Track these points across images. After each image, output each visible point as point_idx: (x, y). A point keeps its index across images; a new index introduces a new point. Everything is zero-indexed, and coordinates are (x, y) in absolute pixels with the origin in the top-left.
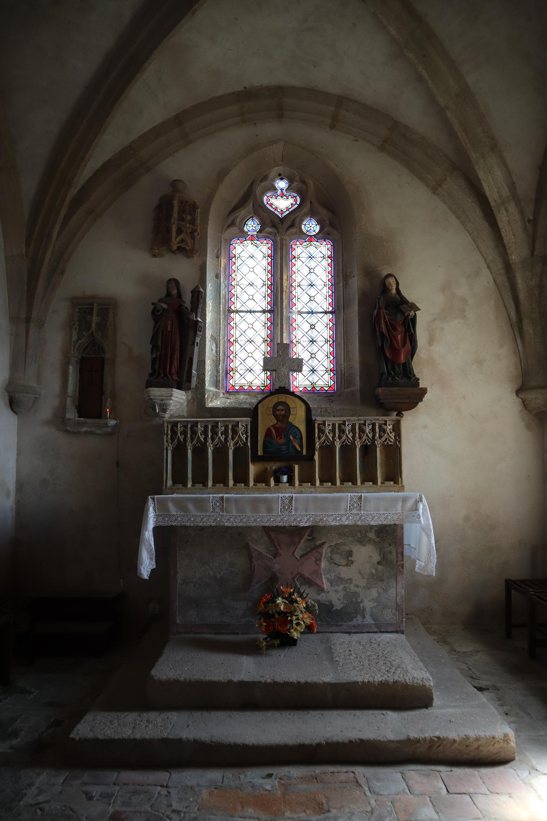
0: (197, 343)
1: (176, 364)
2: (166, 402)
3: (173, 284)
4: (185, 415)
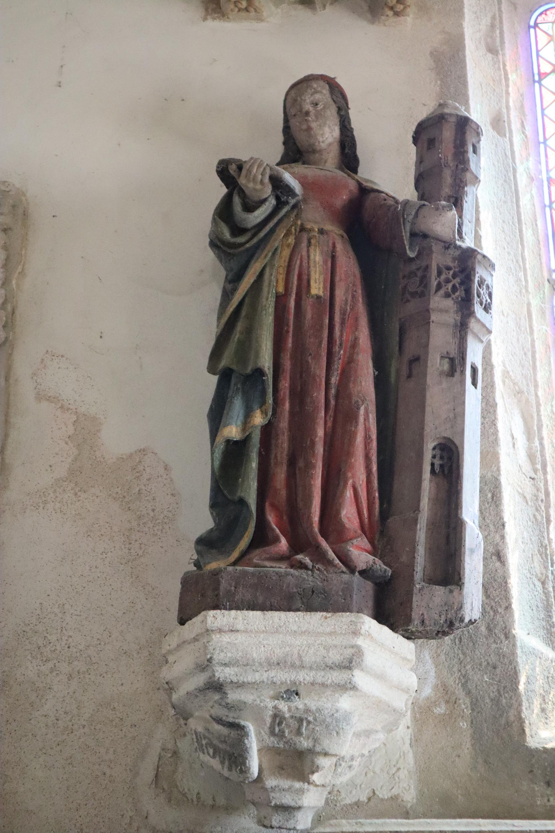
0: (474, 370)
1: (360, 473)
2: (306, 702)
3: (323, 95)
4: (410, 797)
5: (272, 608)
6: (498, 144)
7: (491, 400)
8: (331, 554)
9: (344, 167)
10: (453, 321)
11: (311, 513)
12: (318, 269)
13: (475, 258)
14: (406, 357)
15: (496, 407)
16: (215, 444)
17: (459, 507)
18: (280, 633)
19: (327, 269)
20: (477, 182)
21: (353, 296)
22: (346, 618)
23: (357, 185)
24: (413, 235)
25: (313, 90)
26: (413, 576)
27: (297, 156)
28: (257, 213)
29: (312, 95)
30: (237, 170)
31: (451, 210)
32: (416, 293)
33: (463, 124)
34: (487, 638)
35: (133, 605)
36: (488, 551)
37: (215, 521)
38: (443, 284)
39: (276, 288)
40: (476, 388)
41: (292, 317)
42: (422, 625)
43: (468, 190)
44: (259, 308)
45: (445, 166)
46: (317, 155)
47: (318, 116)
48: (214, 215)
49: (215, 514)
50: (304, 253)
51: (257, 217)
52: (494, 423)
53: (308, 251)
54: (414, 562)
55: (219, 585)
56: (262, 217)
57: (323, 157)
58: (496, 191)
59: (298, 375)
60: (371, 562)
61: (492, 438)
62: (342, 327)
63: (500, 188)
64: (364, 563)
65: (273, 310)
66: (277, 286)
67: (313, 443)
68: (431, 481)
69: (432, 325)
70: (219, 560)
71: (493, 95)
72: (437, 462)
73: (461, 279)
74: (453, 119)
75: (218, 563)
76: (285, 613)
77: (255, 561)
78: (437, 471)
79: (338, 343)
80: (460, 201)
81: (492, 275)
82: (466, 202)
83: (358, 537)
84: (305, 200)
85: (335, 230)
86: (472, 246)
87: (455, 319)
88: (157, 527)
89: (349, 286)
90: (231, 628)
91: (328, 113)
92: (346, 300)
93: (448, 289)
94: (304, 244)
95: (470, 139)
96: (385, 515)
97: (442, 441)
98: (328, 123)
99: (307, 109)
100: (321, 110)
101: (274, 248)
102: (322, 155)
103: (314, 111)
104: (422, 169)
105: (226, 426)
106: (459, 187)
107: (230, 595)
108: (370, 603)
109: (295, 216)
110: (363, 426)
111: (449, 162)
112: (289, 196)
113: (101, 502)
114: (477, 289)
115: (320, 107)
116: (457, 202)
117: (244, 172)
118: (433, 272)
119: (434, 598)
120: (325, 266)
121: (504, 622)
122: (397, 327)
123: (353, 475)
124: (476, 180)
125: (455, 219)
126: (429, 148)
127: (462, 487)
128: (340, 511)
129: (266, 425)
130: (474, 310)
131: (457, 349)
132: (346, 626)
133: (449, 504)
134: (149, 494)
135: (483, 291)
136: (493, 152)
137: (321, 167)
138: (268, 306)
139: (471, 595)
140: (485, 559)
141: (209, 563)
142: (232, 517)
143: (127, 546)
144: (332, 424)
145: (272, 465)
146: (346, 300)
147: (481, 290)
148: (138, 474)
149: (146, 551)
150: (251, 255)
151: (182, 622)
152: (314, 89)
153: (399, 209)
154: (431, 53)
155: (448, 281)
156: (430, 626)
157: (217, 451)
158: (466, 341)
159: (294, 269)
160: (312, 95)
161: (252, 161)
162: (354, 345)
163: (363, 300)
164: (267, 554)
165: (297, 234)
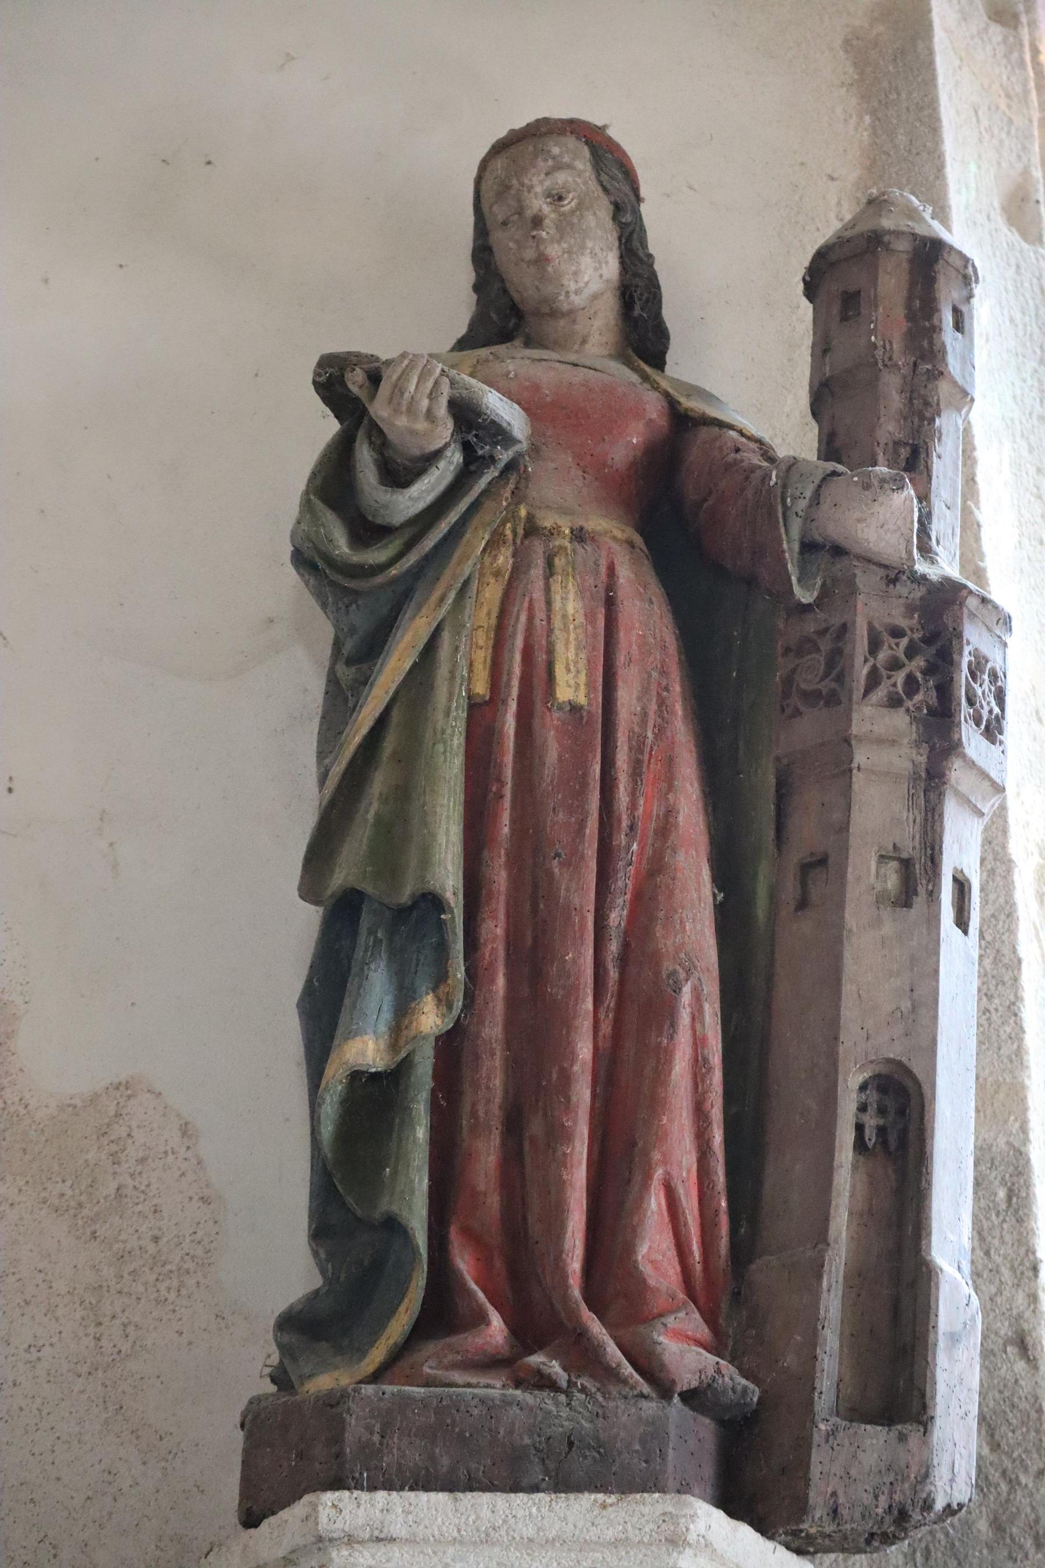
0: (961, 886)
1: (681, 1151)
3: (577, 173)
5: (470, 1486)
6: (1023, 265)
7: (1006, 951)
8: (613, 1352)
9: (630, 352)
10: (909, 765)
11: (562, 1252)
12: (572, 636)
14: (795, 856)
15: (1019, 969)
17: (924, 1234)
18: (493, 1544)
19: (595, 636)
20: (966, 403)
21: (661, 703)
22: (650, 1506)
23: (665, 404)
24: (809, 547)
25: (550, 163)
26: (811, 1403)
27: (511, 325)
28: (415, 490)
29: (547, 174)
30: (367, 384)
31: (901, 488)
33: (929, 257)
34: (991, 1548)
35: (110, 1478)
36: (996, 1334)
37: (323, 1272)
38: (884, 673)
40: (965, 932)
41: (509, 759)
42: (834, 1519)
44: (429, 734)
45: (885, 366)
46: (562, 322)
47: (566, 225)
48: (307, 493)
49: (323, 1256)
50: (538, 595)
52: (1013, 1010)
53: (547, 589)
54: (814, 1367)
55: (344, 1429)
56: (430, 498)
58: (1018, 392)
59: (528, 907)
60: (711, 1372)
63: (1029, 382)
64: (694, 1373)
65: (462, 740)
67: (566, 1080)
68: (855, 1167)
69: (858, 778)
70: (337, 1368)
71: (1008, 133)
72: (871, 1121)
74: (903, 246)
75: (336, 1374)
76: (505, 1495)
77: (426, 1370)
78: (870, 1145)
79: (625, 823)
80: (923, 456)
83: (678, 1309)
84: (535, 450)
85: (610, 527)
87: (913, 762)
88: (167, 1283)
89: (650, 676)
90: (376, 1533)
91: (590, 220)
92: (645, 714)
93: (894, 685)
94: (537, 572)
95: (947, 294)
96: (743, 1253)
98: (589, 244)
100: (573, 212)
101: (465, 577)
102: (574, 321)
103: (553, 216)
106: (922, 418)
107: (369, 1453)
108: (709, 1470)
109: (513, 493)
111: (895, 357)
112: (497, 443)
113: (21, 1219)
115: (569, 204)
116: (914, 460)
118: (858, 645)
119: (861, 1455)
120: (594, 627)
121: (1033, 1508)
122: (772, 780)
123: (664, 1155)
124: (964, 397)
125: (913, 511)
126: (844, 318)
127: (929, 1183)
128: (634, 1245)
129: (449, 1032)
130: (960, 739)
131: (917, 837)
132: (651, 1526)
133: (900, 1225)
134: (142, 1197)
135: (983, 689)
136: (1010, 288)
137: (572, 357)
138: (449, 731)
139: (950, 1445)
140: (986, 1353)
141: (310, 1376)
142: (366, 1263)
143: (91, 1330)
144: (613, 1029)
145: (465, 1131)
146: (645, 714)
147: (976, 686)
148: (114, 1148)
149: (138, 1343)
150: (403, 596)
151: (251, 1519)
152: (554, 158)
153: (772, 483)
154: (847, 42)
155: (895, 665)
156: (852, 1521)
157: (328, 1100)
159: (513, 636)
160: (547, 174)
161: (406, 362)
162: (665, 828)
163: (685, 710)
164: (458, 1353)
165: (518, 542)
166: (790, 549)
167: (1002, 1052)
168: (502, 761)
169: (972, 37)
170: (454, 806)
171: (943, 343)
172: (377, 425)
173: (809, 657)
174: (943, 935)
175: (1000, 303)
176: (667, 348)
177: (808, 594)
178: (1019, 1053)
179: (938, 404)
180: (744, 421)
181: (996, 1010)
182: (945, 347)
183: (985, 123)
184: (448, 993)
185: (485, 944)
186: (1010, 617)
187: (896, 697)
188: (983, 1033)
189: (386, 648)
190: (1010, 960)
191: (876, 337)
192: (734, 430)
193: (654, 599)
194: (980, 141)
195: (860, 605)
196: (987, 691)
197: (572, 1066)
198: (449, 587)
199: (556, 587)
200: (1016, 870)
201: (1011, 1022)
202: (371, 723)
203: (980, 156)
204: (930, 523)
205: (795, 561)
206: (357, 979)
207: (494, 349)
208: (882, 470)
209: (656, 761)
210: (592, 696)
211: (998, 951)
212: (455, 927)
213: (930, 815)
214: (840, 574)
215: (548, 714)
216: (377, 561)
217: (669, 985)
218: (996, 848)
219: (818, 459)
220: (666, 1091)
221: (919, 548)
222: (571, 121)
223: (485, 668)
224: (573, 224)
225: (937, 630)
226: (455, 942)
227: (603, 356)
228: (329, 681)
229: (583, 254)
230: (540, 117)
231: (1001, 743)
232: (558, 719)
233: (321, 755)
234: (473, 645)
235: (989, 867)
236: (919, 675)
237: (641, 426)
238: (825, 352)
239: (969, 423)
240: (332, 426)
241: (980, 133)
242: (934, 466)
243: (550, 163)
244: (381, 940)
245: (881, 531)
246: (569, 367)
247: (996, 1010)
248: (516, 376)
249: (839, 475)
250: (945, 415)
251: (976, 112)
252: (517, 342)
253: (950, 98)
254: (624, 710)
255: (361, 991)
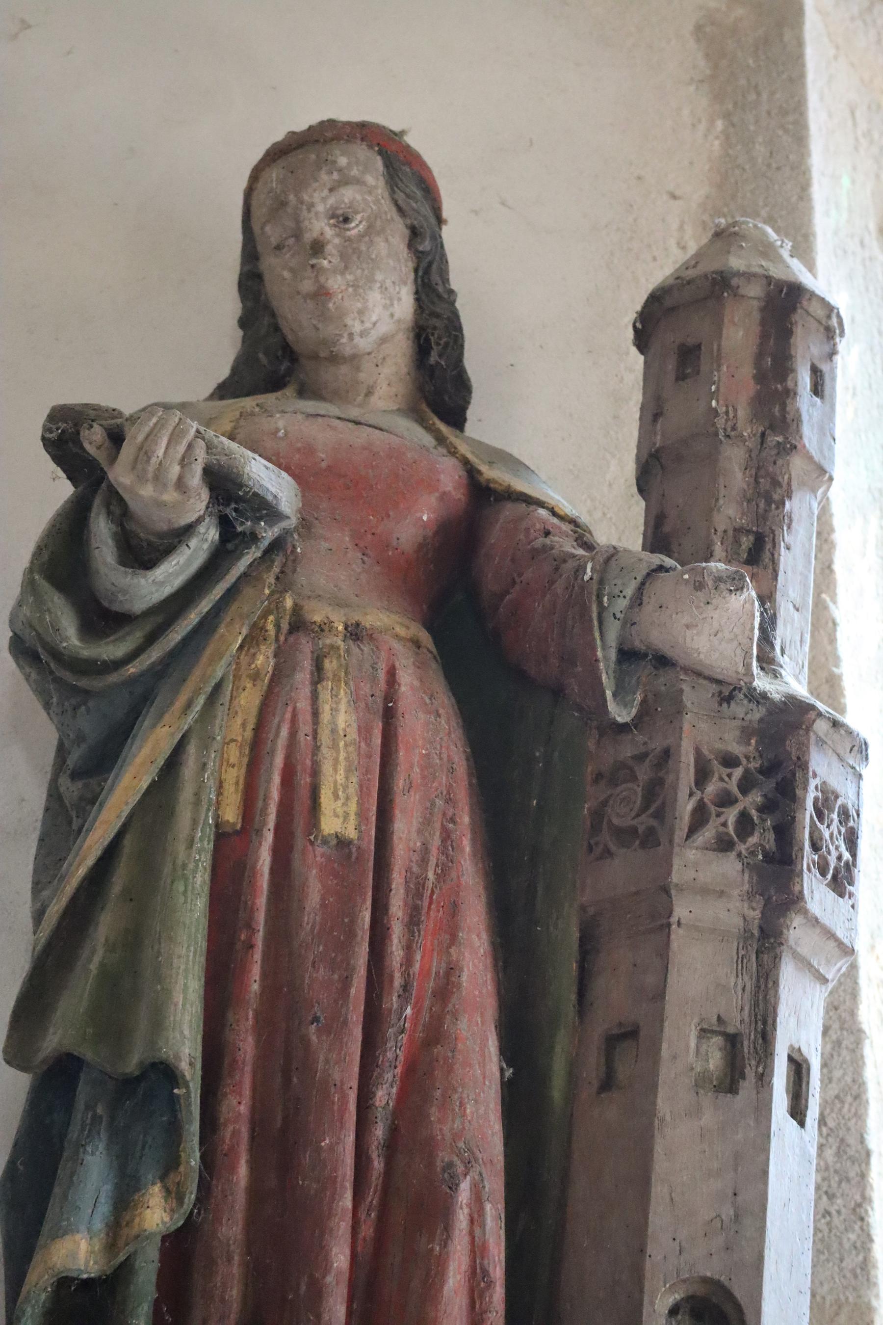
0: (798, 1068)
3: (366, 188)
7: (851, 1140)
9: (424, 406)
12: (342, 755)
13: (808, 730)
14: (601, 1024)
15: (868, 1163)
16: (25, 1289)
21: (446, 835)
23: (463, 473)
24: (628, 655)
28: (161, 571)
29: (331, 190)
30: (107, 443)
32: (634, 831)
33: (786, 307)
38: (713, 809)
39: (217, 809)
40: (802, 1124)
41: (262, 901)
43: (796, 510)
44: (167, 869)
46: (344, 369)
47: (351, 253)
48: (30, 570)
50: (303, 705)
51: (162, 584)
52: (859, 1213)
53: (315, 697)
56: (178, 582)
57: (362, 376)
59: (279, 1079)
61: (852, 1261)
62: (412, 933)
65: (207, 877)
66: (218, 802)
67: (317, 1293)
69: (677, 936)
73: (765, 796)
74: (754, 291)
79: (398, 981)
80: (769, 546)
81: (860, 776)
82: (788, 548)
84: (305, 525)
85: (392, 624)
86: (800, 689)
89: (433, 804)
91: (381, 247)
93: (725, 824)
94: (303, 676)
95: (805, 349)
97: (700, 1290)
98: (379, 277)
99: (315, 234)
100: (361, 236)
102: (358, 369)
103: (337, 241)
104: (658, 441)
105: (59, 1233)
106: (769, 501)
109: (277, 578)
110: (466, 1240)
111: (739, 425)
112: (260, 519)
114: (814, 829)
115: (356, 228)
116: (758, 552)
117: (127, 451)
118: (682, 775)
120: (364, 742)
122: (575, 934)
124: (821, 474)
125: (753, 615)
126: (681, 377)
129: (179, 1230)
130: (801, 892)
131: (747, 1009)
135: (831, 830)
137: (354, 412)
138: (191, 866)
147: (822, 827)
150: (141, 701)
152: (340, 170)
153: (586, 578)
155: (725, 800)
158: (776, 983)
159: (272, 753)
160: (331, 190)
162: (446, 987)
165: (282, 638)
166: (604, 657)
167: (844, 1264)
168: (254, 903)
169: (852, 19)
170: (195, 956)
171: (798, 411)
172: (117, 492)
173: (624, 785)
174: (774, 1127)
175: (872, 350)
176: (469, 403)
177: (624, 713)
178: (866, 1266)
179: (789, 484)
180: (556, 497)
181: (839, 1212)
182: (800, 416)
183: (863, 126)
184: (178, 1184)
185: (225, 1125)
186: (866, 744)
187: (726, 838)
188: (822, 1240)
189: (120, 761)
190: (857, 1151)
191: (718, 402)
192: (543, 507)
193: (441, 711)
194: (856, 149)
195: (686, 727)
196: (836, 832)
197: (324, 1277)
198: (197, 692)
199: (325, 695)
200: (867, 1042)
201: (857, 1227)
202: (99, 853)
203: (854, 168)
204: (774, 629)
205: (611, 672)
206: (70, 1165)
207: (261, 398)
208: (717, 566)
209: (438, 907)
210: (363, 828)
211: (842, 1140)
212: (190, 1105)
213: (762, 980)
214: (663, 688)
215: (310, 848)
216: (112, 657)
217: (444, 1179)
218: (843, 1015)
219: (644, 548)
220: (437, 1311)
221: (759, 659)
222: (363, 125)
223: (237, 790)
224: (361, 252)
225: (781, 745)
226: (191, 1122)
227: (392, 412)
228: (50, 796)
229: (370, 288)
230: (325, 118)
231: (851, 895)
232: (322, 855)
233: (37, 887)
234: (223, 761)
235: (834, 1037)
236: (754, 813)
237: (433, 500)
238: (656, 416)
239: (828, 499)
240: (64, 490)
241: (857, 139)
242: (782, 558)
243: (335, 176)
244: (101, 1117)
245: (715, 641)
246: (350, 425)
247: (839, 1212)
248: (286, 434)
249: (667, 570)
250: (797, 496)
251: (853, 113)
252: (289, 391)
253: (822, 99)
254: (401, 846)
255: (75, 1178)
